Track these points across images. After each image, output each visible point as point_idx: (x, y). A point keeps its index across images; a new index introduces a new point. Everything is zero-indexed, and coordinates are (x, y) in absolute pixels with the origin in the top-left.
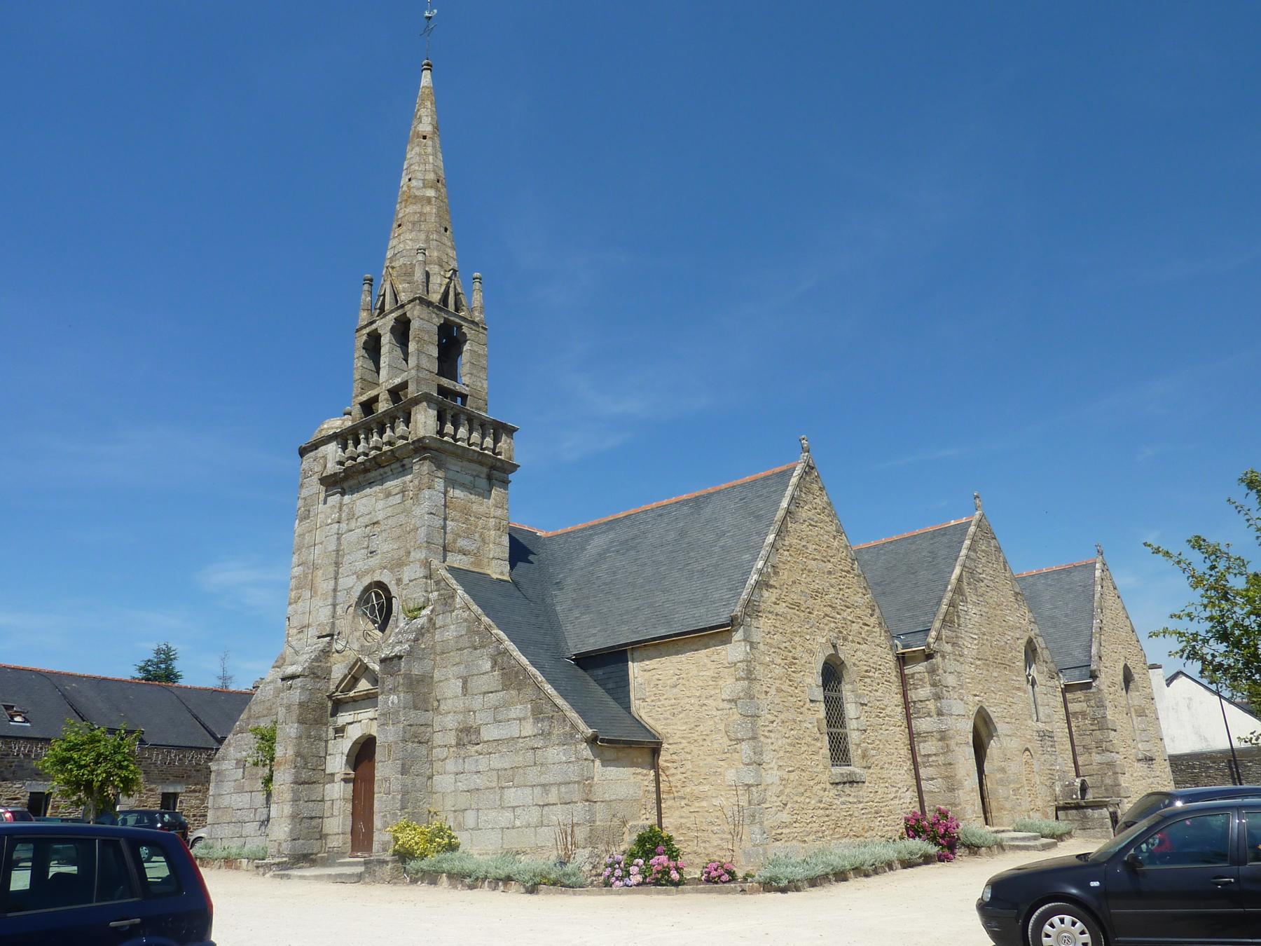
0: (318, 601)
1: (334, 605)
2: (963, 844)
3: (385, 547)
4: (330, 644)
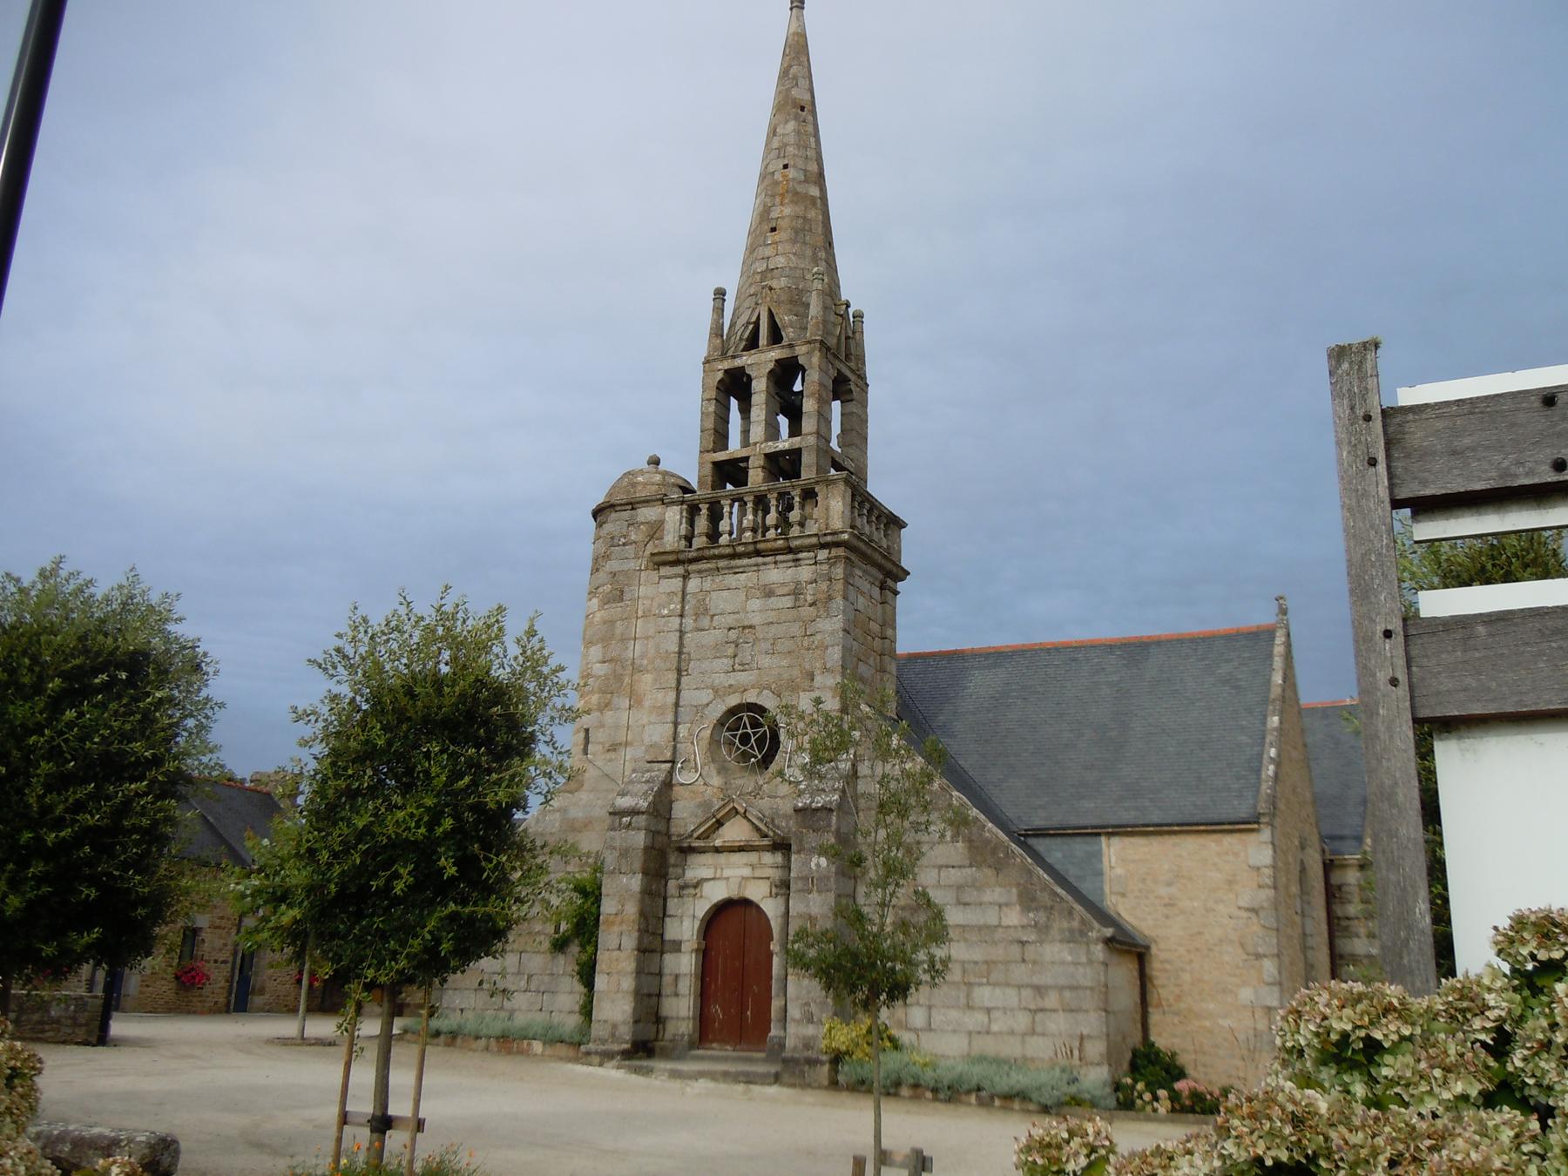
0: (642, 716)
1: (676, 724)
2: (1094, 1104)
3: (772, 665)
4: (671, 773)
